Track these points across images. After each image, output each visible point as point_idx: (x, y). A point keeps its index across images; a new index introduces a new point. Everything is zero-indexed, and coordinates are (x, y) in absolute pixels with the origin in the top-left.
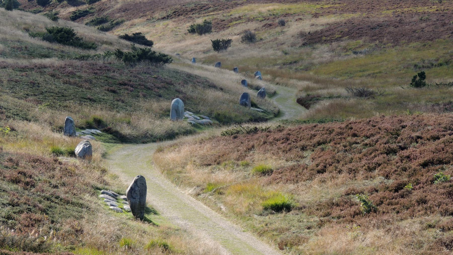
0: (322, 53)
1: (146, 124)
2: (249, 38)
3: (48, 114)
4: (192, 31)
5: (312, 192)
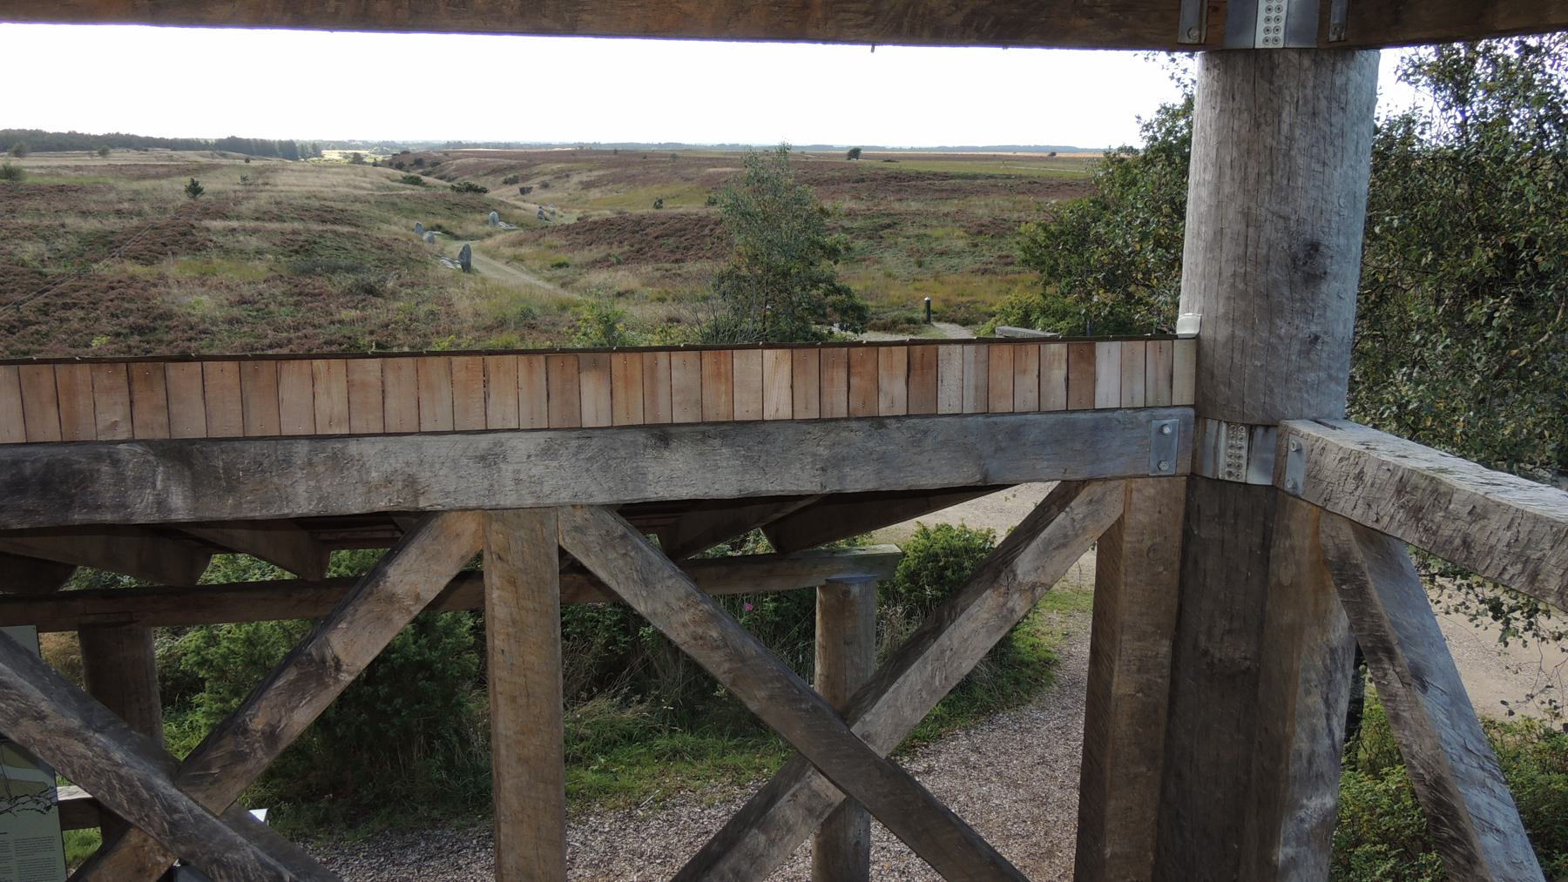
0: (595, 193)
1: (472, 228)
2: (545, 186)
3: (404, 221)
4: (506, 182)
5: (580, 256)
